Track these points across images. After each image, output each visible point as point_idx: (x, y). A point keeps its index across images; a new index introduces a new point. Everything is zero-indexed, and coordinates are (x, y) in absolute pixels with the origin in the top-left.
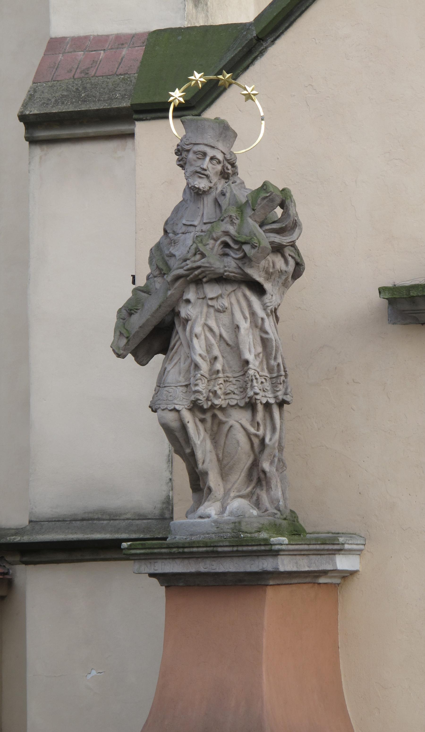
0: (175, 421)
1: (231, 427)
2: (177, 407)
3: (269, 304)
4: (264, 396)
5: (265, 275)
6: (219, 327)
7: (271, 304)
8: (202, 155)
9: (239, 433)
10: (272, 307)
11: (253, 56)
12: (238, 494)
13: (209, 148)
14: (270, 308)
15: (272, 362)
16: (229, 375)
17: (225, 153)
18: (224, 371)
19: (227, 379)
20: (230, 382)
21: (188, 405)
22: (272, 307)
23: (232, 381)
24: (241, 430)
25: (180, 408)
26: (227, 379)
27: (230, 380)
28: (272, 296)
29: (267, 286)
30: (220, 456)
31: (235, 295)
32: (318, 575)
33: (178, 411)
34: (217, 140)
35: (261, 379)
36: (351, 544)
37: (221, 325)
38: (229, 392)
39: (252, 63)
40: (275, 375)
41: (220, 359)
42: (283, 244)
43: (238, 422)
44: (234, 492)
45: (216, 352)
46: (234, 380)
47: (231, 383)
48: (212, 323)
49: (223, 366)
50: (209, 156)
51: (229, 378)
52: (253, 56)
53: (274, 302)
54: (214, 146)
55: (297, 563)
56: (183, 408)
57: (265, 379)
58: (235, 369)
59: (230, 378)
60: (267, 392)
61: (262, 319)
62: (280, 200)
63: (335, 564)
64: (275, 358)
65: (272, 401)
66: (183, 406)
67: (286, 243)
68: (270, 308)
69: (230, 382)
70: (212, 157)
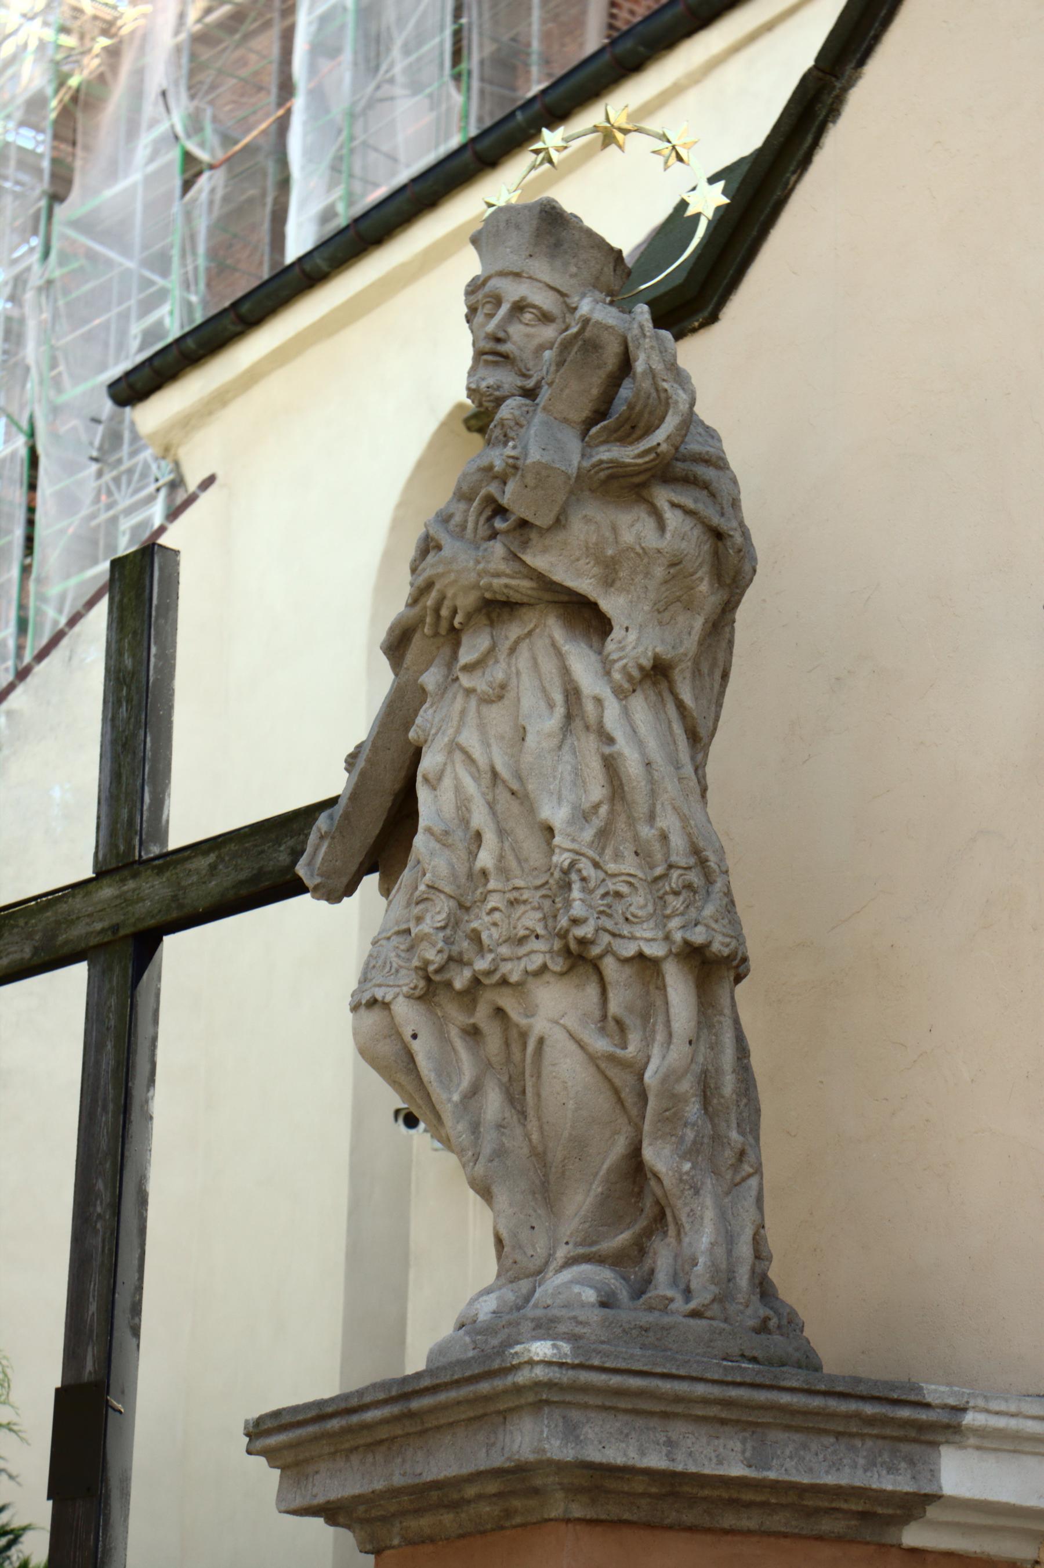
0: (385, 1038)
1: (541, 1041)
2: (379, 994)
3: (614, 656)
4: (630, 935)
5: (596, 570)
6: (486, 744)
7: (622, 654)
8: (536, 316)
9: (566, 1056)
10: (625, 661)
11: (817, 123)
12: (581, 1250)
13: (511, 278)
14: (618, 665)
15: (646, 832)
16: (519, 883)
17: (563, 290)
18: (503, 871)
19: (515, 894)
20: (525, 902)
21: (412, 985)
22: (625, 661)
23: (530, 900)
24: (572, 1046)
25: (387, 996)
26: (515, 894)
27: (525, 897)
28: (627, 629)
29: (610, 604)
30: (535, 1137)
31: (531, 649)
32: (891, 1516)
33: (386, 1006)
34: (527, 254)
35: (614, 884)
36: (997, 1413)
37: (492, 741)
38: (522, 932)
39: (816, 144)
40: (659, 871)
41: (490, 838)
42: (623, 462)
43: (557, 1023)
44: (567, 1243)
45: (480, 818)
46: (534, 897)
47: (529, 907)
48: (470, 739)
49: (501, 858)
50: (508, 300)
51: (520, 891)
52: (817, 123)
53: (630, 647)
54: (518, 271)
55: (670, 1443)
56: (398, 994)
57: (630, 884)
58: (537, 864)
59: (522, 891)
60: (637, 923)
61: (599, 701)
62: (617, 342)
63: (934, 1474)
64: (652, 817)
65: (656, 950)
66: (397, 990)
67: (633, 458)
68: (618, 665)
69: (525, 902)
70: (518, 301)
